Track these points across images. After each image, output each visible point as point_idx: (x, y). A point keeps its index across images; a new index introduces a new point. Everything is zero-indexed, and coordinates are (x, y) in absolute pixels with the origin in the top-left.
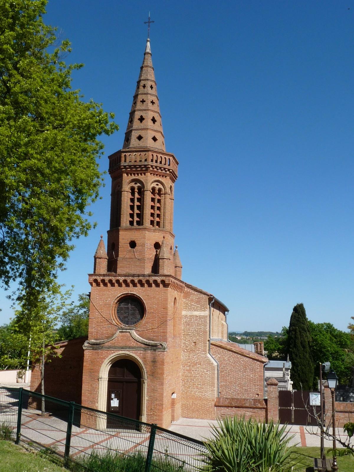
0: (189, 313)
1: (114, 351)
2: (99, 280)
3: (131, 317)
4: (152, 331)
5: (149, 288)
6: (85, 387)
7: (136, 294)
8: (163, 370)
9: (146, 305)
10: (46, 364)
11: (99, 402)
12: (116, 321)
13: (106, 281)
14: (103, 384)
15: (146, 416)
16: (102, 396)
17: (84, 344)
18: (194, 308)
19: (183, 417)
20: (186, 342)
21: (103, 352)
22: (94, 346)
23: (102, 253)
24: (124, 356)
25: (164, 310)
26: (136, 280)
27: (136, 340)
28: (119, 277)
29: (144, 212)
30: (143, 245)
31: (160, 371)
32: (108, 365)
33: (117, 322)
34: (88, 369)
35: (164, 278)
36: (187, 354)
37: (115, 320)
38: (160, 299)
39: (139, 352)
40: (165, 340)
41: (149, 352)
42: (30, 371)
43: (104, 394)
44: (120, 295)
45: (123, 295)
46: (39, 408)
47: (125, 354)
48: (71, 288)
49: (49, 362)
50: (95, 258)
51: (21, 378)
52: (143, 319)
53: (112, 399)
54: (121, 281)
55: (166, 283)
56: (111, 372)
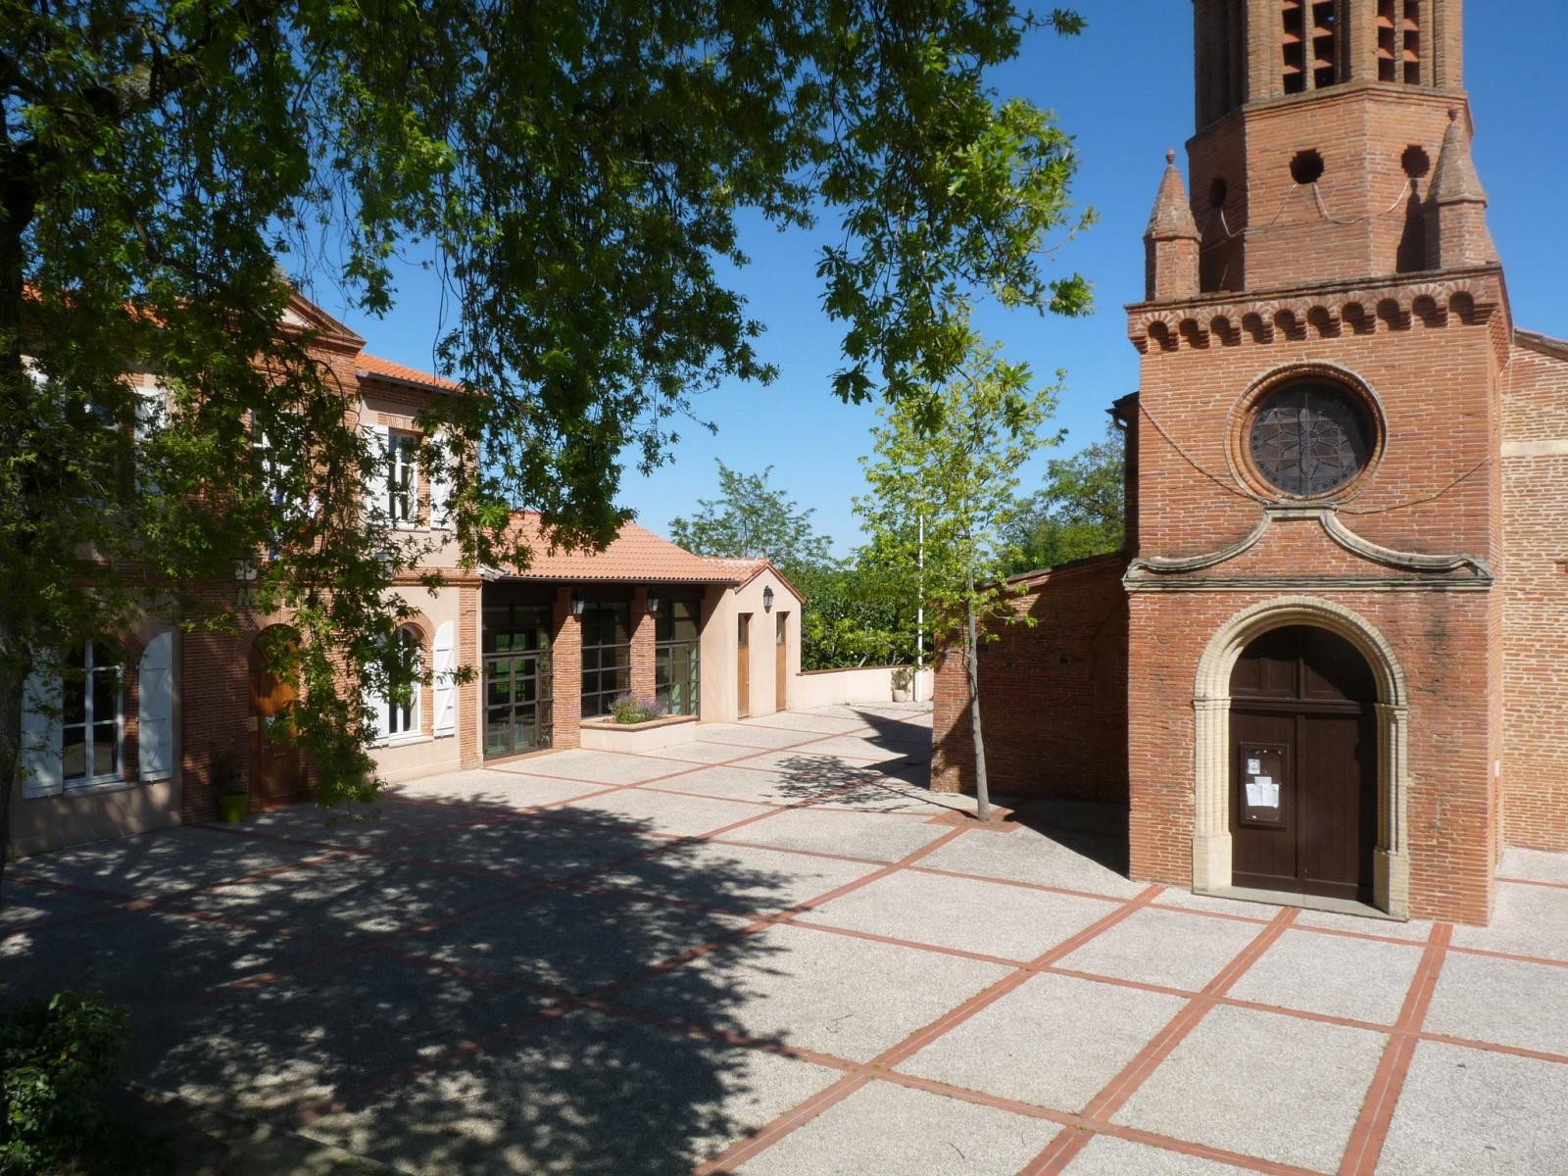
0: (1532, 448)
1: (1255, 595)
2: (1172, 325)
3: (1315, 463)
4: (1414, 513)
5: (1392, 333)
6: (1139, 732)
7: (1335, 365)
8: (1482, 667)
9: (1382, 408)
10: (982, 647)
11: (1201, 790)
12: (1250, 480)
13: (1202, 327)
14: (1210, 721)
15: (1407, 851)
16: (1210, 765)
17: (1125, 570)
18: (1553, 427)
19: (1516, 844)
20: (1523, 564)
21: (1205, 600)
22: (1168, 577)
23: (1179, 219)
24: (1296, 613)
25: (1469, 419)
26: (1334, 305)
27: (1350, 551)
28: (1259, 304)
29: (1353, 24)
30: (1356, 161)
31: (1466, 675)
32: (1229, 650)
33: (1256, 485)
34: (1150, 665)
35: (1464, 284)
36: (1529, 608)
37: (1247, 475)
38: (1449, 375)
39: (1366, 595)
40: (1482, 546)
41: (1413, 595)
42: (931, 672)
43: (1219, 760)
44: (1265, 374)
45: (1275, 373)
46: (968, 788)
47: (1304, 606)
48: (1055, 381)
49: (992, 641)
50: (1150, 243)
51: (904, 687)
52: (1372, 463)
53: (1252, 779)
54: (1266, 318)
55: (1476, 302)
56: (1240, 678)
